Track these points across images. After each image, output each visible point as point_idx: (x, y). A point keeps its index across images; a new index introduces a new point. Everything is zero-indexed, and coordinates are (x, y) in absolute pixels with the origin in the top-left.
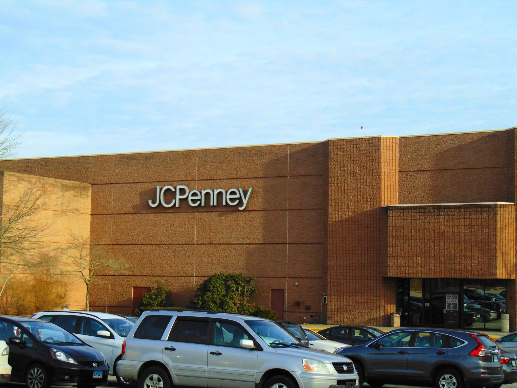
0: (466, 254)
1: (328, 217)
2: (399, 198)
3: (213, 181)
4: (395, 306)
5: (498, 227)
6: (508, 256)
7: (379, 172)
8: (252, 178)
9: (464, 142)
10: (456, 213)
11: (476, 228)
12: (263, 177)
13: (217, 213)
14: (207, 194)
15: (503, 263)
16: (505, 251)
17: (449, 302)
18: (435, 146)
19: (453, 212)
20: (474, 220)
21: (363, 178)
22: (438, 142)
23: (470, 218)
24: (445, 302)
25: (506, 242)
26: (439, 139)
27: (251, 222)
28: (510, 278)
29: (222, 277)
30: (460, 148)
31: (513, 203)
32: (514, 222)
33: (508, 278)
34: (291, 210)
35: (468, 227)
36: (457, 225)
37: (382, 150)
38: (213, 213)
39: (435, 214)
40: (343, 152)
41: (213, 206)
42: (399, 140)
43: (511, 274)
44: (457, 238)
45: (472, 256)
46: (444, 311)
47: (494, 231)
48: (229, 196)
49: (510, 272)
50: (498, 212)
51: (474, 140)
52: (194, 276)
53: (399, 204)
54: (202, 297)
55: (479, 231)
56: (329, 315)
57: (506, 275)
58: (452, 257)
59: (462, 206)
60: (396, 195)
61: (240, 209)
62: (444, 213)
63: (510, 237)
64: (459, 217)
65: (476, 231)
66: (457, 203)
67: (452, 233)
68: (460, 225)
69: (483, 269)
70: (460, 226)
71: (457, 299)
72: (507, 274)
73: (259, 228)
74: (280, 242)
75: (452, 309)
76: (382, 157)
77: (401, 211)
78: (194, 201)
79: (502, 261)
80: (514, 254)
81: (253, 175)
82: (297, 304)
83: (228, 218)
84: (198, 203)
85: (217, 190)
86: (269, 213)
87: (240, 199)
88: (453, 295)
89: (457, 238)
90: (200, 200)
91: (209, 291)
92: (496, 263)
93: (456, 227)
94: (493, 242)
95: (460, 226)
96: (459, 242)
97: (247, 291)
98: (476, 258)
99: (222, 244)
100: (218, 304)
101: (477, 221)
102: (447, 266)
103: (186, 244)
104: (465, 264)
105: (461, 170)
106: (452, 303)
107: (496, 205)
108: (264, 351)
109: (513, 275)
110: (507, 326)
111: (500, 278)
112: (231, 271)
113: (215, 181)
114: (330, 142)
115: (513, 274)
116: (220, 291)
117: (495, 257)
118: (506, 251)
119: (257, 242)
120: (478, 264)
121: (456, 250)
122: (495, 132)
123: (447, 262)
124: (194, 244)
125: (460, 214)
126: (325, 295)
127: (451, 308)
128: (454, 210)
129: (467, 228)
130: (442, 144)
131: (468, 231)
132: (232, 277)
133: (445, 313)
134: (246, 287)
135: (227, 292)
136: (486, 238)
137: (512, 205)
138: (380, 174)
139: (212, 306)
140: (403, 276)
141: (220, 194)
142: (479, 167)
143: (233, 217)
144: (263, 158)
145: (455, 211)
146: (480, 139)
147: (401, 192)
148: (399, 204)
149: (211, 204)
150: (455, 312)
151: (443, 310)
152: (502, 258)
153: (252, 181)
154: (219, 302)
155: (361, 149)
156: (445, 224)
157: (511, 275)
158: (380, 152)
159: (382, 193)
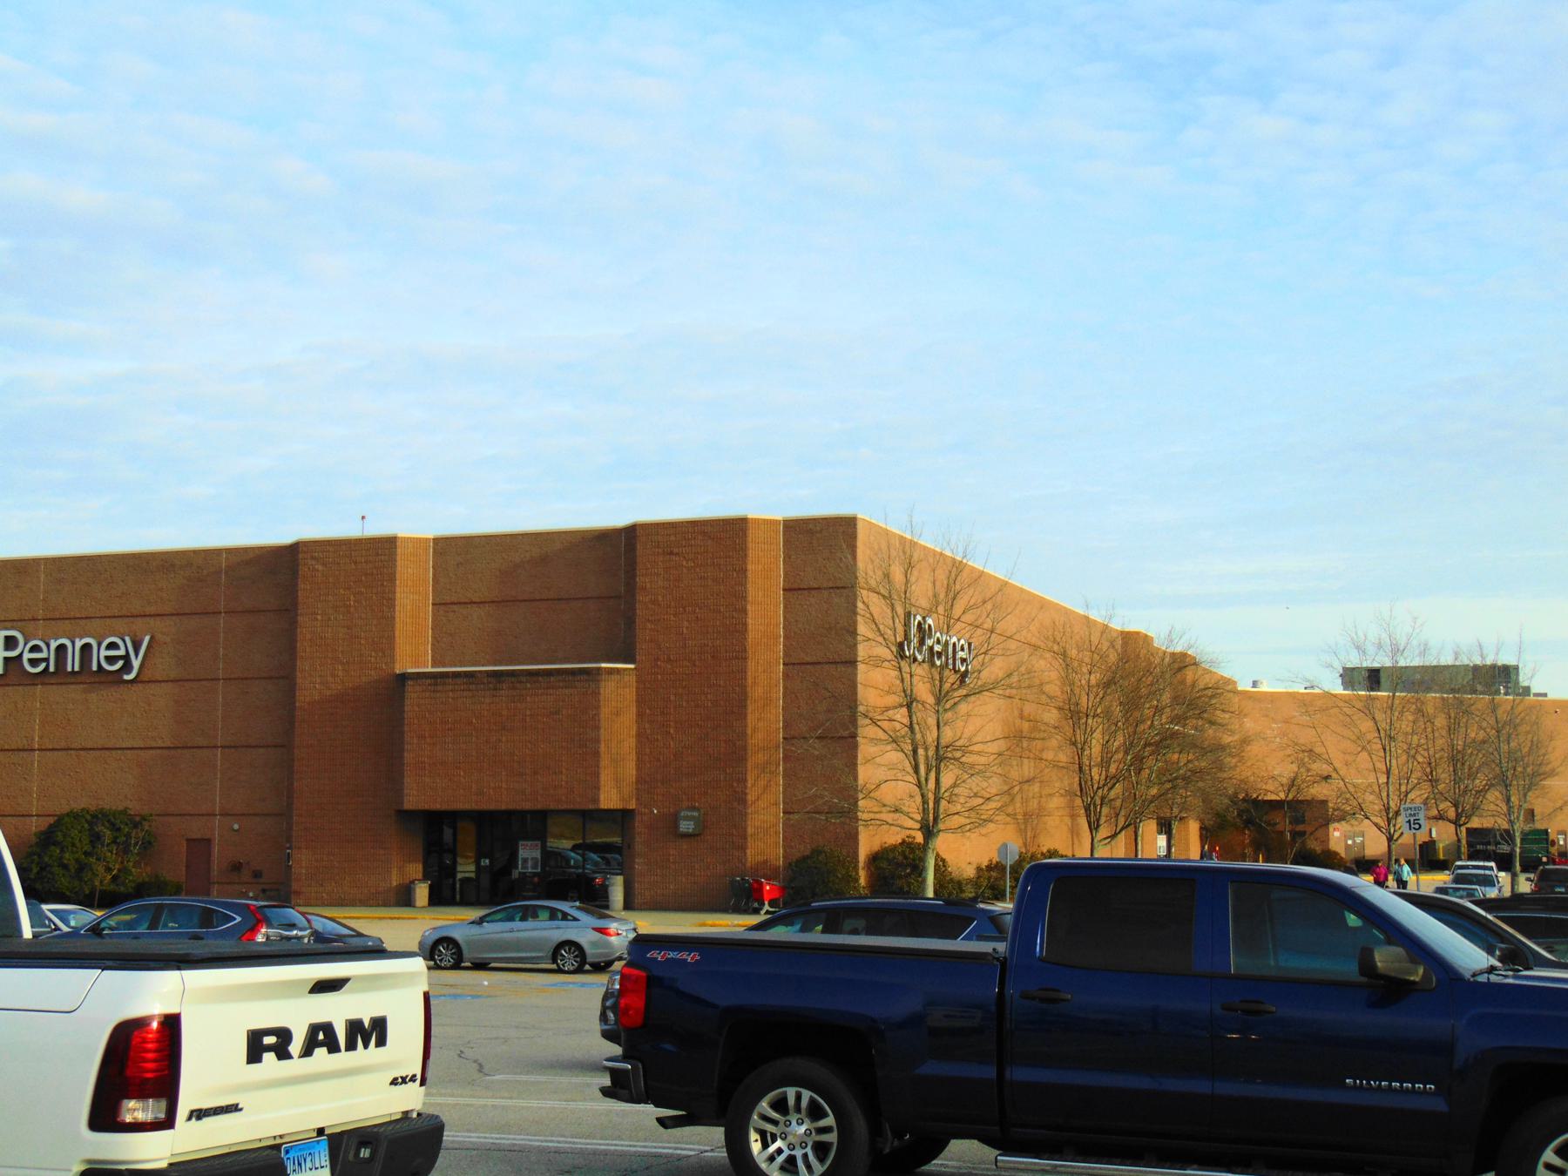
1: (295, 694)
2: (432, 656)
3: (73, 621)
4: (421, 866)
7: (391, 603)
8: (150, 616)
12: (172, 615)
13: (82, 686)
14: (61, 649)
17: (525, 856)
21: (363, 616)
27: (149, 705)
29: (83, 816)
31: (632, 666)
34: (226, 679)
37: (398, 563)
38: (73, 687)
39: (491, 686)
40: (324, 564)
41: (73, 672)
42: (434, 543)
48: (104, 653)
52: (33, 816)
53: (432, 667)
54: (39, 856)
56: (295, 886)
61: (126, 677)
73: (164, 716)
74: (205, 743)
76: (398, 576)
77: (429, 681)
78: (33, 662)
81: (151, 610)
82: (237, 867)
83: (103, 696)
84: (43, 665)
85: (81, 639)
86: (184, 686)
87: (126, 658)
90: (46, 660)
91: (55, 844)
97: (136, 844)
98: (564, 771)
99: (90, 749)
100: (73, 871)
103: (19, 750)
106: (530, 857)
107: (599, 669)
112: (110, 803)
113: (77, 621)
114: (301, 545)
116: (78, 845)
119: (160, 744)
120: (567, 782)
124: (35, 750)
126: (288, 848)
127: (527, 868)
132: (105, 815)
133: (517, 876)
134: (133, 834)
135: (94, 847)
137: (630, 669)
138: (394, 608)
139: (58, 875)
140: (1027, 773)
141: (86, 648)
143: (112, 695)
144: (172, 576)
147: (436, 644)
148: (432, 667)
149: (69, 669)
150: (535, 874)
153: (152, 621)
154: (73, 867)
155: (358, 559)
158: (395, 566)
159: (397, 646)
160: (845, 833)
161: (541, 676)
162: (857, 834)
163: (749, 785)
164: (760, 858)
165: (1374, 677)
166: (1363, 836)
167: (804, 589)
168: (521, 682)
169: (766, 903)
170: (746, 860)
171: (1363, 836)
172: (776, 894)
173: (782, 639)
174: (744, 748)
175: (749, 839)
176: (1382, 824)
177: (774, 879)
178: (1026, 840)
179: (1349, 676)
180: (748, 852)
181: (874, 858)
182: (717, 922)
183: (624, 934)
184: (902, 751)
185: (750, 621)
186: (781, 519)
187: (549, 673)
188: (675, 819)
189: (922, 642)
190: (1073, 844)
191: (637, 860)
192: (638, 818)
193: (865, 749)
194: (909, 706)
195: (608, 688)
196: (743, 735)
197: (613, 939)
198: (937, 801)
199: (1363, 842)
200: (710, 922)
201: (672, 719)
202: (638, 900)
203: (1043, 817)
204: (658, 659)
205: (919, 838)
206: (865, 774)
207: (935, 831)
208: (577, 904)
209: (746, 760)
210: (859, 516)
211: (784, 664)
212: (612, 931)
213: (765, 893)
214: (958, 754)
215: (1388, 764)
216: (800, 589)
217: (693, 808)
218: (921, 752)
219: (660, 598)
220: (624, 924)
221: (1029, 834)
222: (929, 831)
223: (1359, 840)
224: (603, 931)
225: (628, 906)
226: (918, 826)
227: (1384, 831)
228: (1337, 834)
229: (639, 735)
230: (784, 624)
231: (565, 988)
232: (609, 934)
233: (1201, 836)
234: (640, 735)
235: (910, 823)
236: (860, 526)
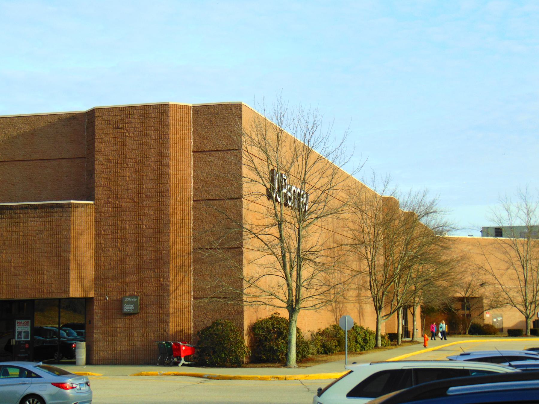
0: (32, 268)
5: (73, 233)
6: (85, 269)
9: (37, 126)
10: (21, 215)
11: (45, 233)
15: (78, 278)
16: (81, 262)
17: (20, 330)
18: (3, 131)
19: (18, 214)
20: (44, 224)
22: (6, 126)
23: (39, 221)
24: (15, 329)
25: (83, 251)
26: (7, 122)
28: (87, 296)
30: (33, 134)
31: (92, 202)
32: (94, 225)
33: (85, 296)
35: (36, 233)
36: (22, 230)
43: (89, 291)
44: (22, 247)
45: (41, 269)
46: (13, 342)
47: (67, 238)
49: (87, 288)
50: (73, 213)
51: (49, 123)
55: (49, 238)
57: (82, 293)
58: (16, 272)
59: (28, 206)
60: (189, 232)
62: (7, 216)
63: (87, 244)
64: (25, 220)
65: (45, 237)
66: (19, 202)
67: (16, 241)
68: (27, 230)
69: (53, 285)
70: (27, 232)
71: (29, 325)
72: (83, 291)
75: (23, 338)
79: (76, 275)
80: (93, 266)
88: (25, 321)
89: (22, 247)
92: (69, 278)
93: (21, 234)
94: (66, 251)
95: (27, 232)
96: (24, 252)
98: (45, 272)
101: (47, 225)
102: (10, 284)
104: (32, 281)
105: (34, 162)
106: (23, 331)
107: (69, 204)
108: (317, 397)
109: (91, 293)
110: (83, 357)
111: (74, 296)
115: (91, 291)
117: (67, 270)
118: (83, 262)
121: (21, 262)
122: (75, 114)
123: (10, 279)
125: (27, 217)
128: (19, 212)
129: (35, 234)
130: (10, 129)
131: (35, 237)
133: (14, 343)
136: (57, 247)
137: (91, 204)
142: (55, 158)
145: (20, 213)
146: (57, 122)
150: (27, 342)
151: (12, 340)
152: (76, 270)
156: (8, 230)
157: (88, 292)
160: (235, 311)
161: (31, 209)
162: (242, 312)
163: (171, 280)
164: (178, 329)
165: (499, 232)
166: (502, 317)
167: (207, 151)
168: (16, 213)
169: (183, 358)
170: (169, 330)
171: (502, 317)
172: (189, 352)
173: (192, 185)
174: (168, 255)
175: (171, 316)
176: (524, 311)
177: (188, 342)
178: (337, 317)
179: (485, 231)
180: (170, 324)
181: (253, 328)
182: (150, 373)
183: (78, 387)
184: (274, 254)
185: (171, 172)
186: (191, 105)
187: (35, 207)
188: (121, 303)
189: (279, 191)
190: (360, 320)
191: (95, 331)
192: (96, 303)
193: (248, 255)
194: (280, 225)
195: (75, 217)
196: (167, 248)
197: (69, 391)
198: (298, 287)
199: (502, 320)
200: (145, 373)
201: (119, 236)
202: (96, 358)
203: (345, 304)
204: (109, 198)
205: (284, 314)
206: (248, 271)
207: (297, 308)
208: (41, 364)
209: (169, 263)
210: (243, 103)
211: (193, 200)
212: (68, 385)
213: (182, 351)
214: (312, 257)
215: (525, 274)
216: (204, 151)
217: (132, 296)
218: (287, 255)
219: (111, 157)
220: (77, 379)
221: (338, 313)
222: (292, 309)
223: (499, 319)
224: (61, 385)
225: (89, 362)
226: (285, 305)
227: (524, 313)
228: (488, 316)
229: (96, 248)
230: (194, 174)
231: (386, 182)
232: (66, 388)
233: (421, 316)
234: (97, 248)
235: (278, 302)
236: (243, 109)
